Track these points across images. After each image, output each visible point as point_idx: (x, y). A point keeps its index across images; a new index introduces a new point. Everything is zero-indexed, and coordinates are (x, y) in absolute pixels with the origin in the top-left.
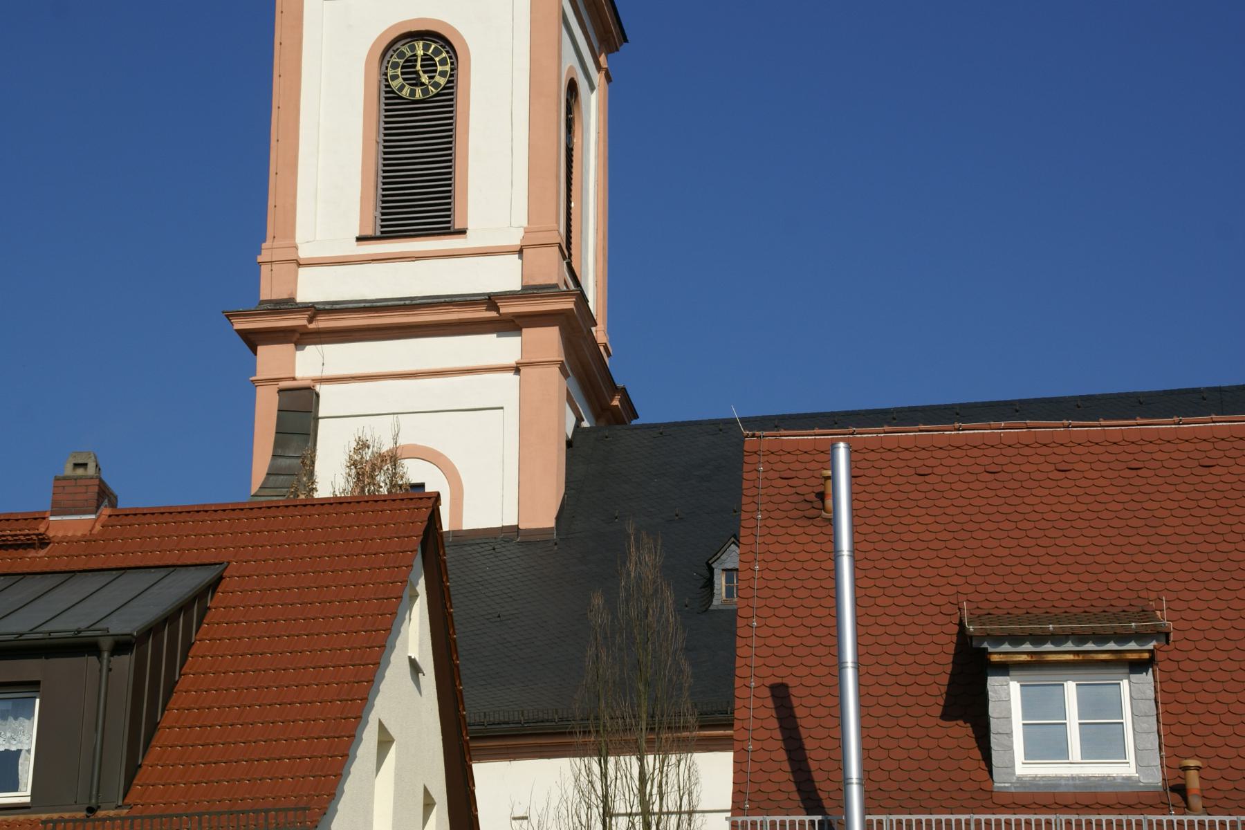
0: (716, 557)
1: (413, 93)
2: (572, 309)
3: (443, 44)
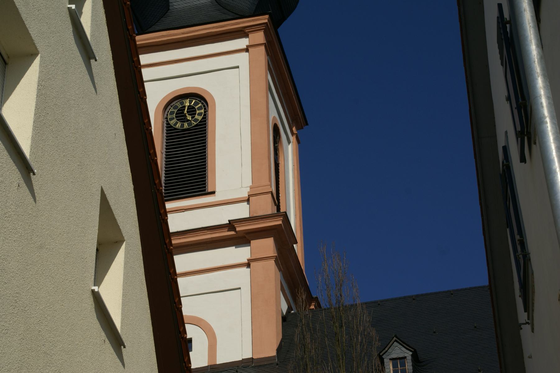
0: (384, 351)
1: (182, 126)
2: (281, 224)
3: (200, 100)
